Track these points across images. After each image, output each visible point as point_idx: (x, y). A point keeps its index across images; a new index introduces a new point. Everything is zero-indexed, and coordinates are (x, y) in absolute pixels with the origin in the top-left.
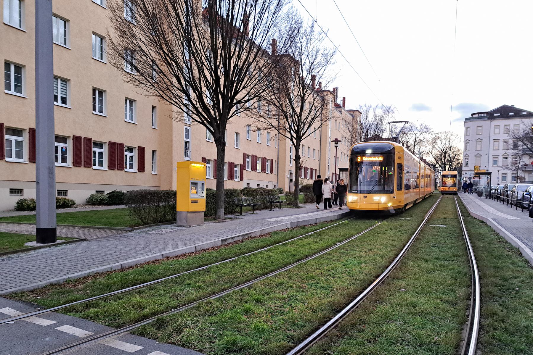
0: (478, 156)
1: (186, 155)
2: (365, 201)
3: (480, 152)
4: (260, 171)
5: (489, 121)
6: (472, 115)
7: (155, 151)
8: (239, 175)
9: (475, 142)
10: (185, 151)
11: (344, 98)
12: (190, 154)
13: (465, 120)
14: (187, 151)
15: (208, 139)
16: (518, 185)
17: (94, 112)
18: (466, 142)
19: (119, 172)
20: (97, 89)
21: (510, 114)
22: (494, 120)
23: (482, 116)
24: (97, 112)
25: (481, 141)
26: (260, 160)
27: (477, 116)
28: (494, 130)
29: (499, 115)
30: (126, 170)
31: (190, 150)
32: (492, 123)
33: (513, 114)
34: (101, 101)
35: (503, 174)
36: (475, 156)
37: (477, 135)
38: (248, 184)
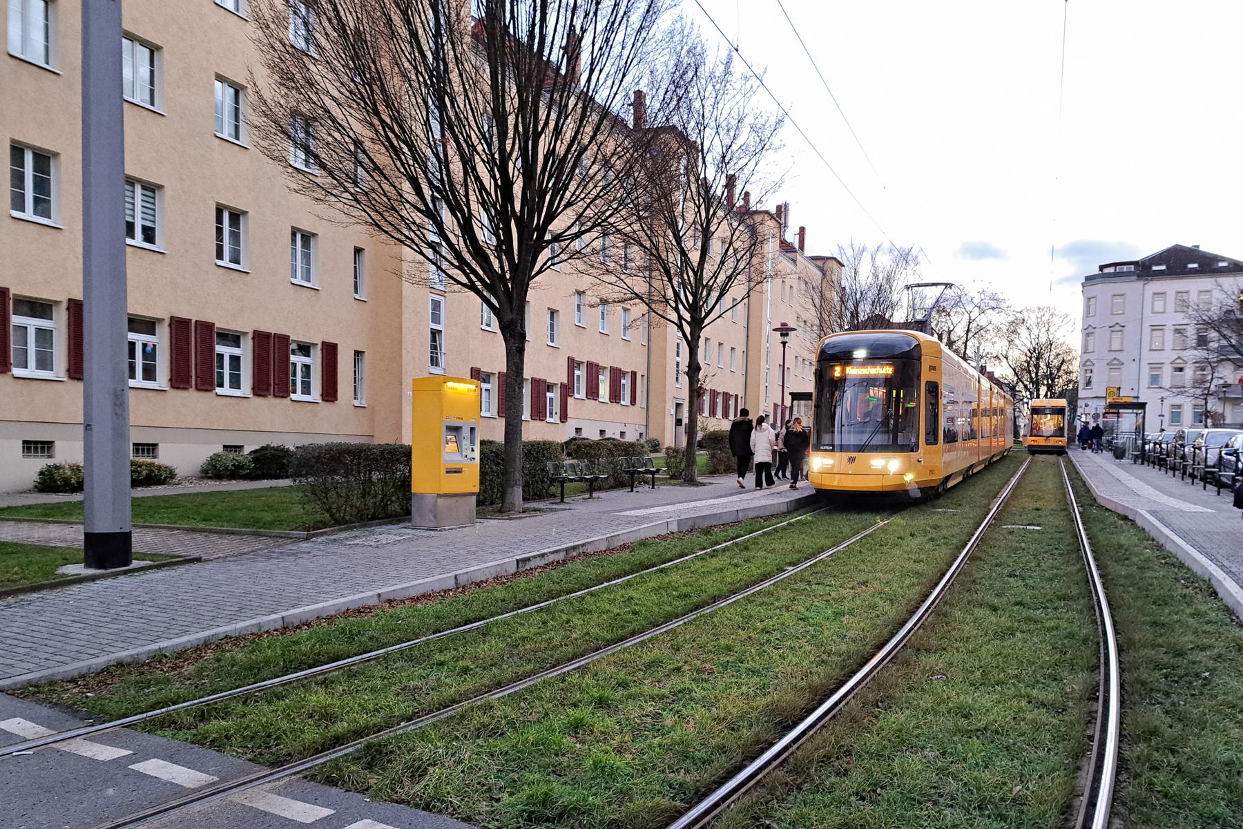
0: (1114, 365)
1: (434, 361)
2: (851, 468)
3: (1118, 356)
4: (607, 400)
5: (1141, 283)
6: (1102, 268)
7: (362, 352)
8: (557, 407)
9: (1107, 331)
10: (431, 353)
11: (802, 230)
12: (442, 360)
13: (1083, 281)
14: (437, 354)
15: (484, 324)
16: (1208, 433)
17: (220, 263)
18: (1088, 332)
19: (278, 401)
20: (226, 207)
21: (1190, 266)
22: (1151, 280)
23: (1125, 270)
24: (226, 262)
25: (1121, 328)
26: (607, 373)
27: (1111, 270)
28: (1153, 304)
29: (1163, 268)
30: (293, 396)
31: (443, 351)
32: (1146, 286)
33: (1195, 265)
34: (235, 237)
36: (1108, 364)
37: (1112, 314)
38: (578, 430)
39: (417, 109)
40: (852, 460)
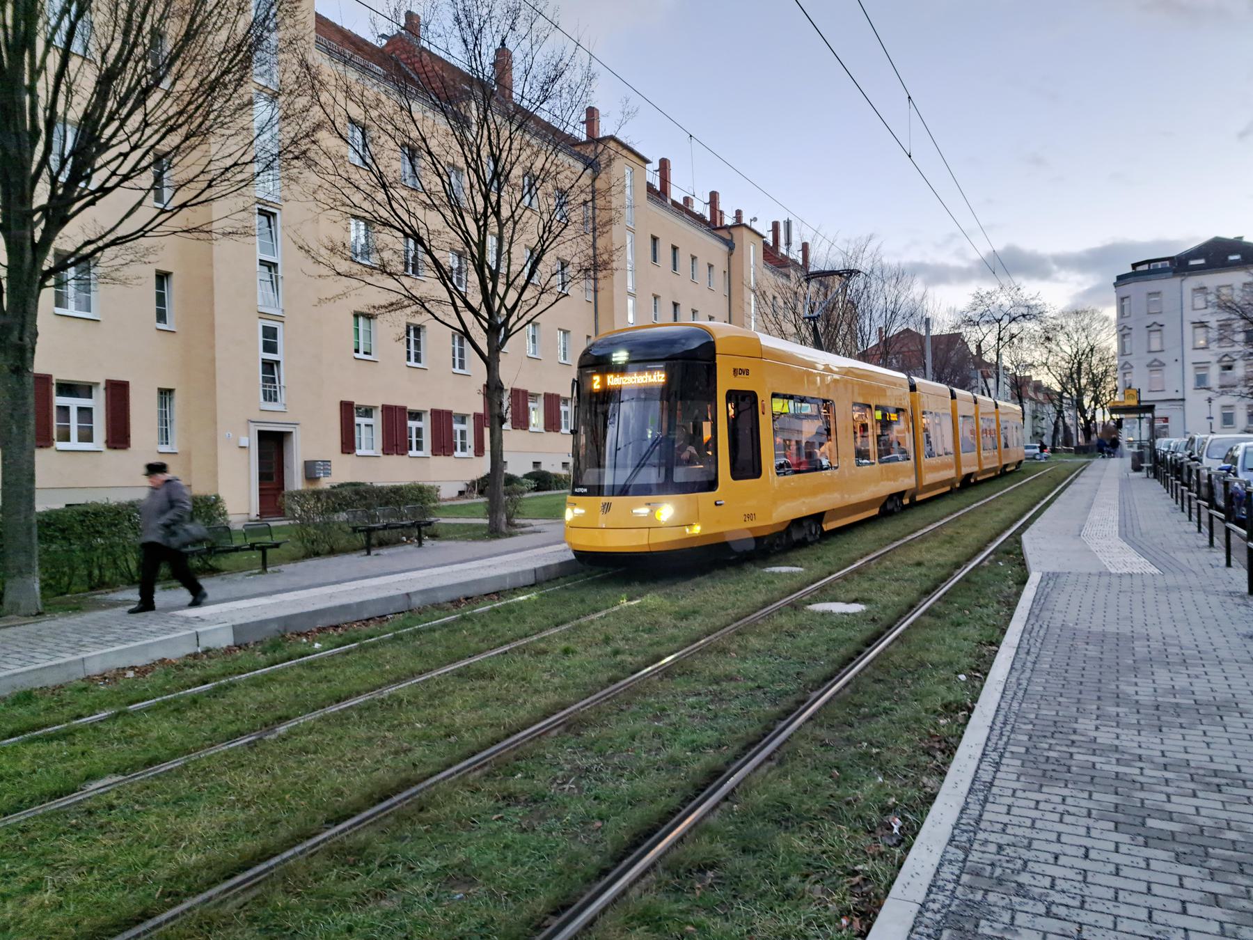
1: (270, 396)
2: (602, 520)
5: (1178, 279)
6: (1134, 266)
7: (171, 391)
8: (470, 440)
10: (264, 386)
11: (714, 196)
12: (282, 397)
14: (275, 387)
15: (361, 351)
17: (409, 364)
18: (1124, 333)
19: (400, 457)
20: (412, 324)
21: (1232, 258)
22: (1190, 275)
24: (71, 310)
27: (1145, 267)
29: (1202, 261)
30: (410, 453)
31: (282, 384)
32: (1185, 283)
33: (1237, 257)
34: (417, 344)
35: (1224, 407)
36: (1148, 366)
38: (536, 464)
39: (1128, 513)
40: (607, 507)
